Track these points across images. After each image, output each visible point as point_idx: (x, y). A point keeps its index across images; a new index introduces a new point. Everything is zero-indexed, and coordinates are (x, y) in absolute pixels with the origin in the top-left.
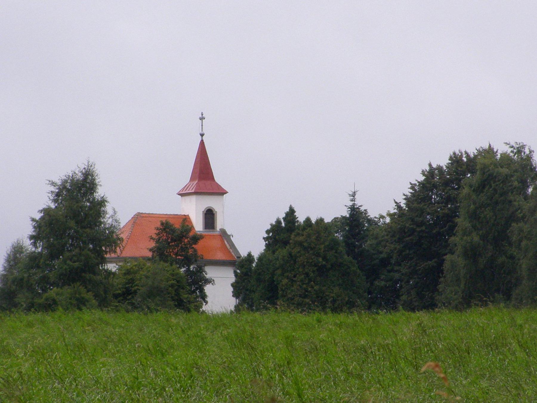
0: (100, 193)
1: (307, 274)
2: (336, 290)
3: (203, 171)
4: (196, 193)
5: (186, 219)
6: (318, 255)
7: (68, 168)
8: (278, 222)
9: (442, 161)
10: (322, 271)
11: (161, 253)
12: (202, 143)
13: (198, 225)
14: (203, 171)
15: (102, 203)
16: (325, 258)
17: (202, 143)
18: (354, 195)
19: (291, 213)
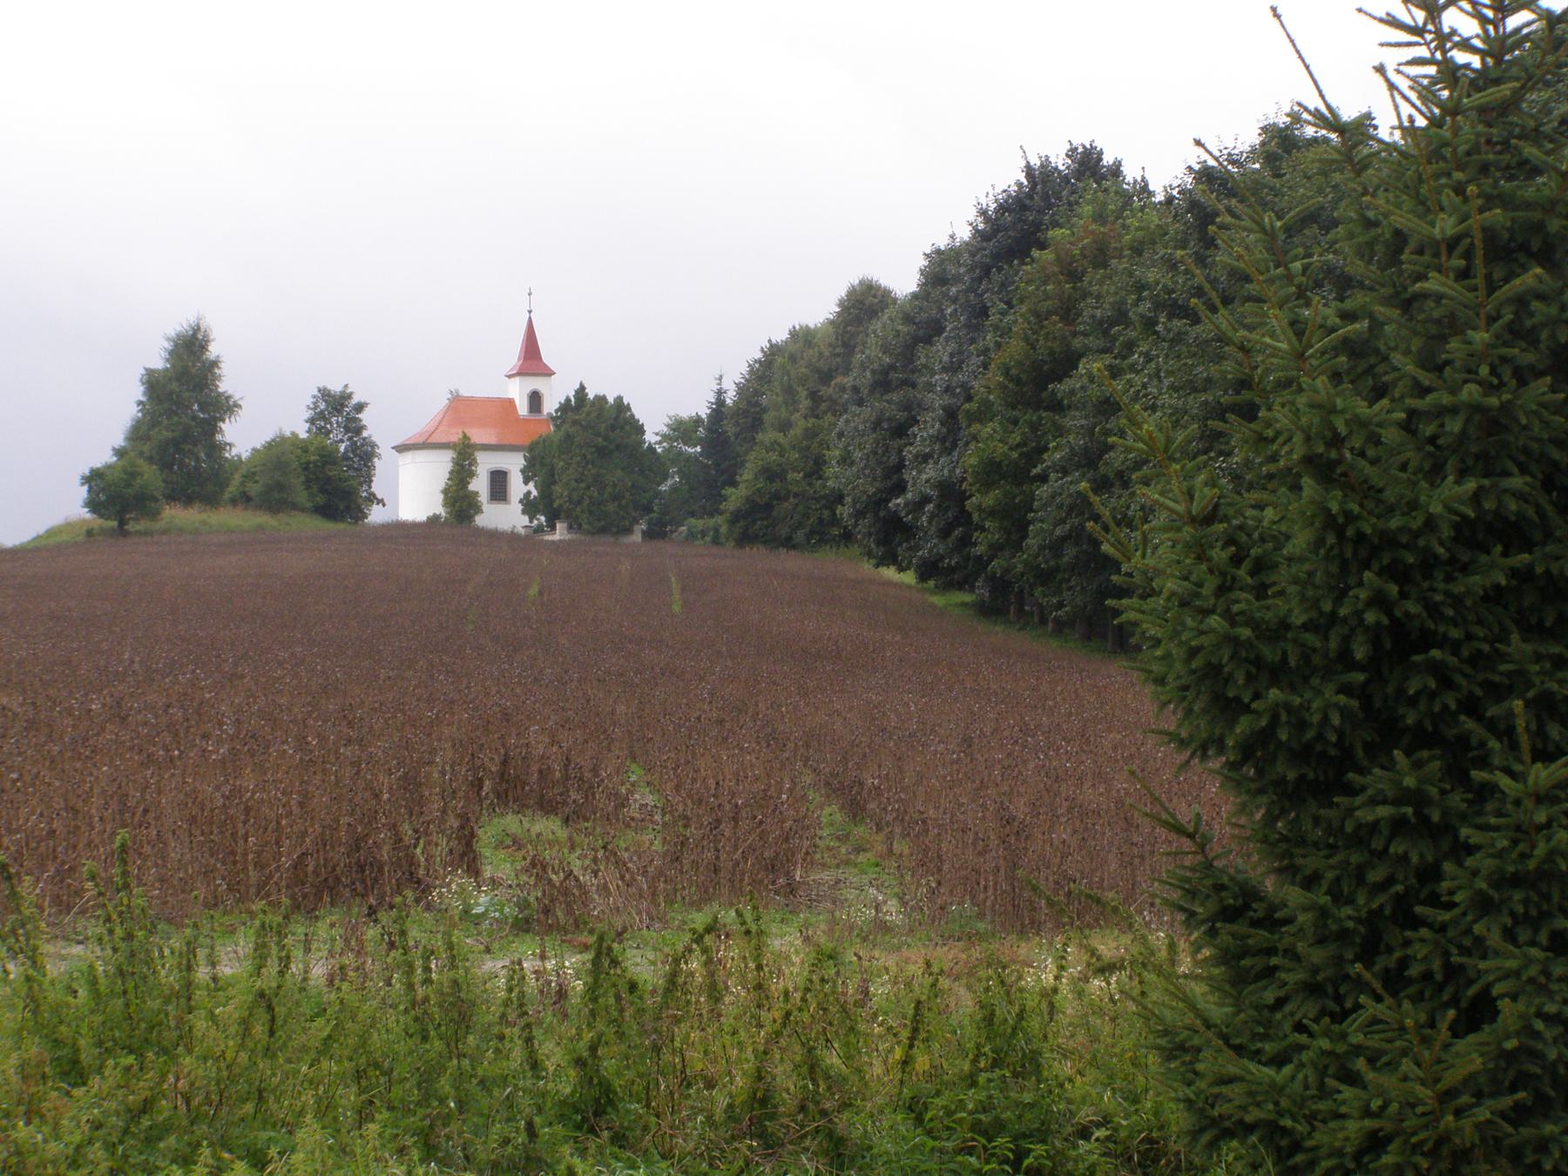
0: (214, 350)
1: (584, 456)
2: (619, 473)
3: (531, 349)
4: (519, 374)
5: (511, 402)
6: (599, 435)
7: (177, 324)
8: (568, 400)
9: (781, 336)
10: (602, 452)
11: (318, 419)
12: (530, 320)
13: (522, 408)
14: (531, 349)
15: (215, 364)
16: (606, 438)
17: (530, 320)
18: (721, 378)
19: (582, 388)
